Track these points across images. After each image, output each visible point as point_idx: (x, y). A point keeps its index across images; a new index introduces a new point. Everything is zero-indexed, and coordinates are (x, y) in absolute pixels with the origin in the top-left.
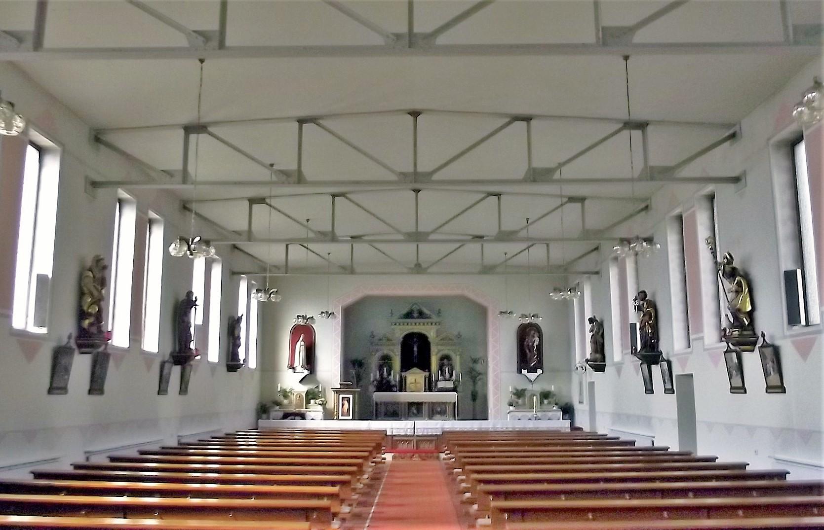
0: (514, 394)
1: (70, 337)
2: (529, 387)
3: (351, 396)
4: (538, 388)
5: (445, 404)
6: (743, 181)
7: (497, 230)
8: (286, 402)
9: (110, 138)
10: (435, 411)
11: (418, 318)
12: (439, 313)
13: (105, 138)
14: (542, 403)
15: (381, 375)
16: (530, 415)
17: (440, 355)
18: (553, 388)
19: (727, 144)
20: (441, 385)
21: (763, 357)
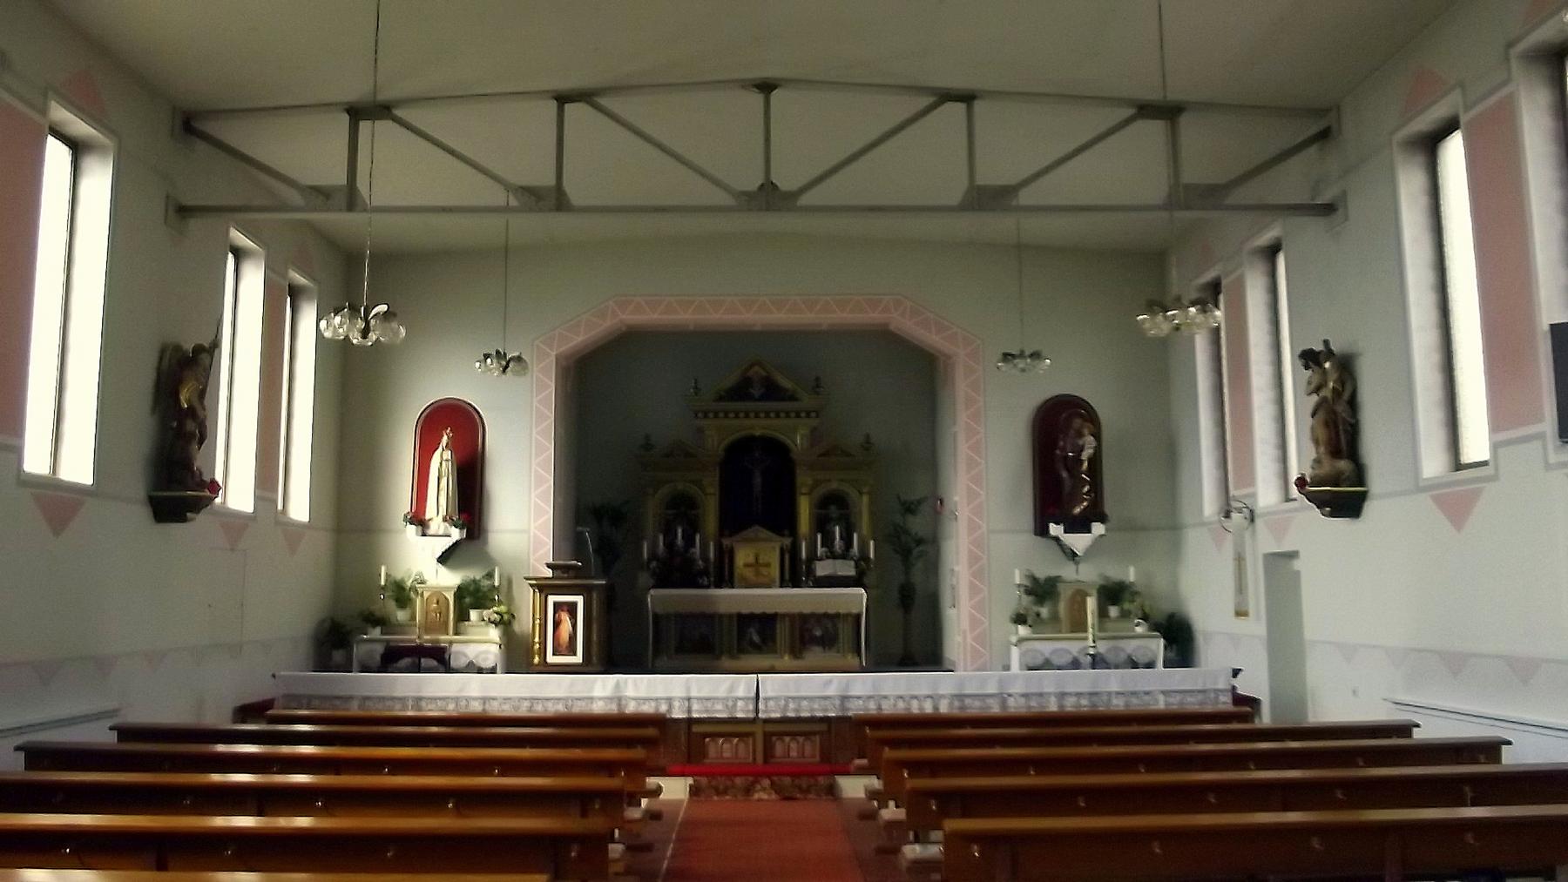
0: (1029, 592)
2: (1068, 572)
3: (579, 600)
4: (1089, 574)
5: (835, 617)
6: (1340, 212)
7: (963, 184)
8: (401, 615)
9: (212, 128)
10: (808, 640)
11: (762, 398)
12: (817, 386)
13: (198, 125)
14: (1102, 614)
15: (670, 545)
16: (1073, 648)
17: (821, 491)
18: (1131, 575)
19: (1313, 150)
20: (823, 569)
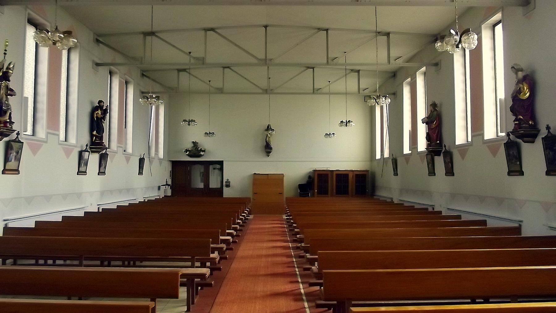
1: (87, 145)
21: (444, 157)
